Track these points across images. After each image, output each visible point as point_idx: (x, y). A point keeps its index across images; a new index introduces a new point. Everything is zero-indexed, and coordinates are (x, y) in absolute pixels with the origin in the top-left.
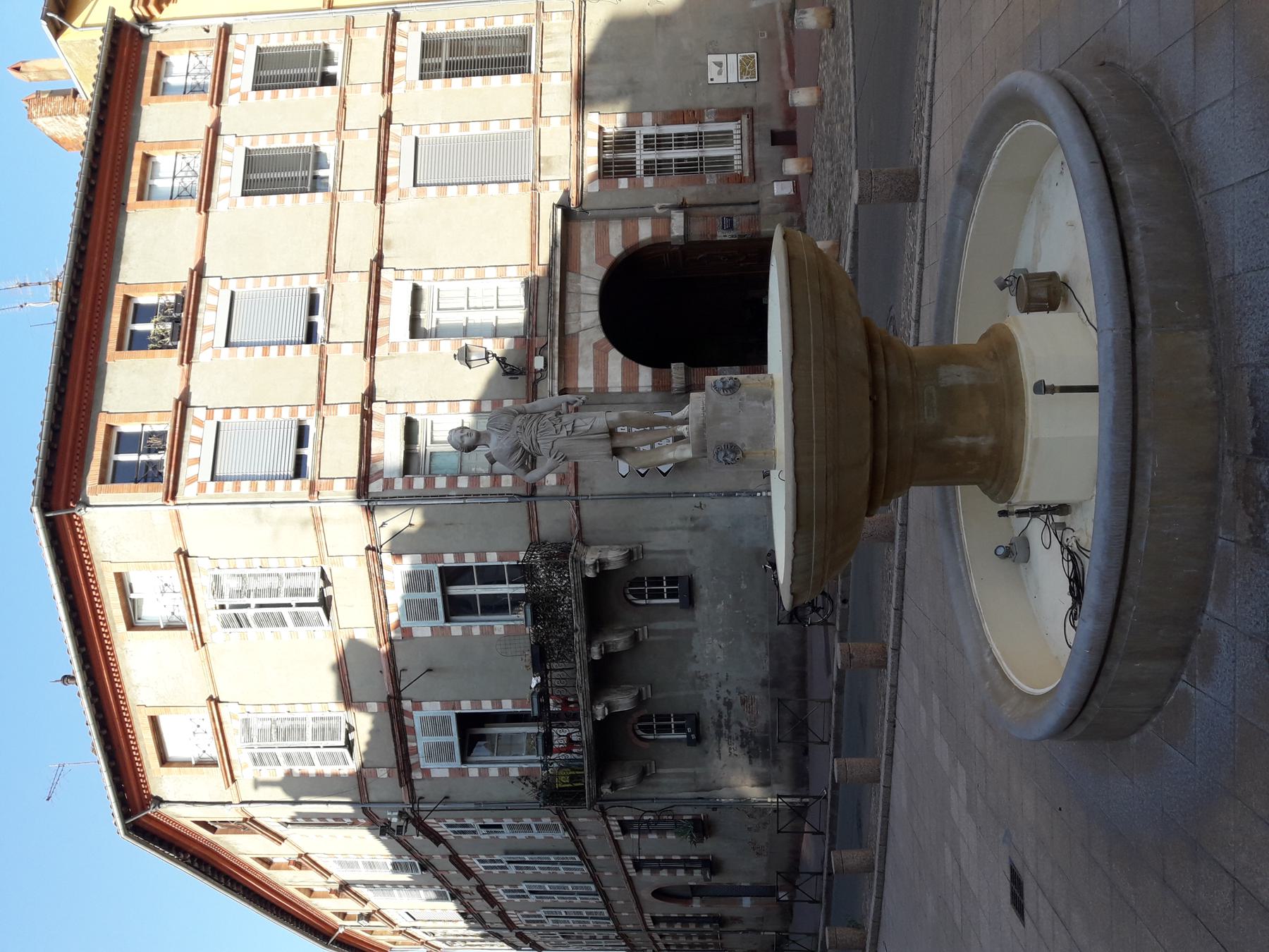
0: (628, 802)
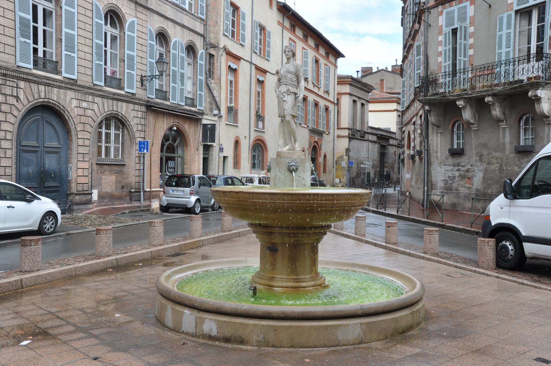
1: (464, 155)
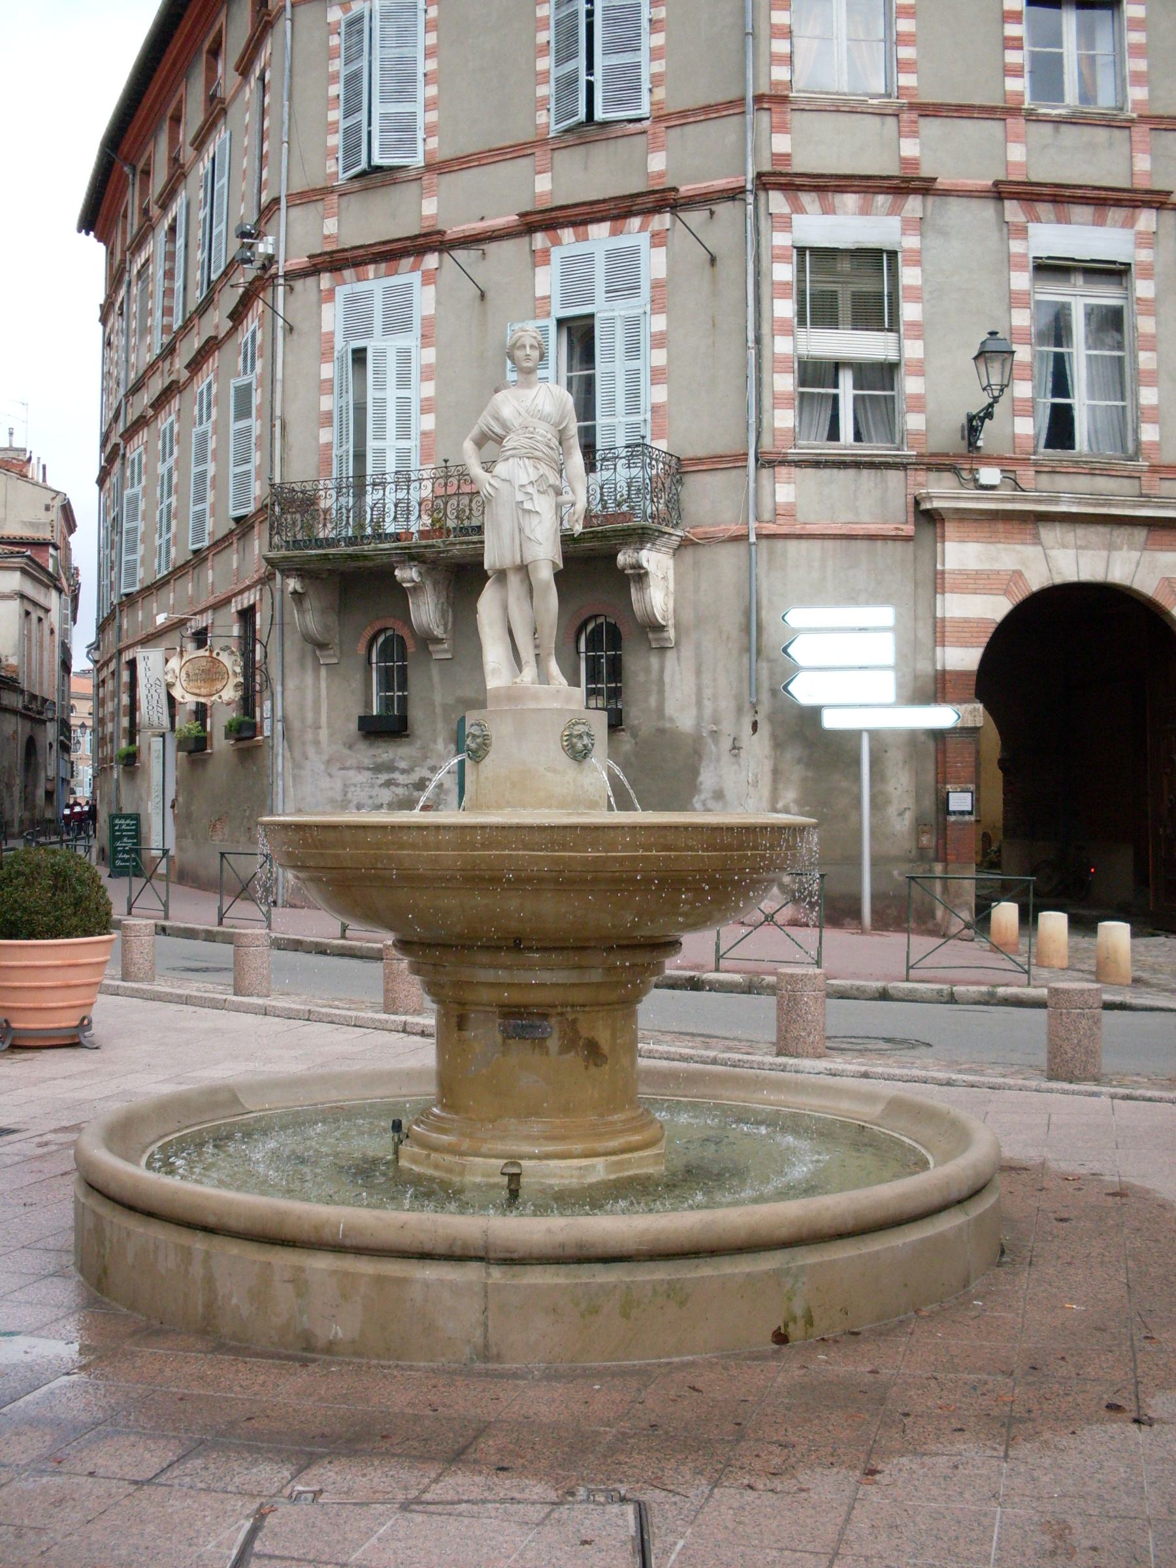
0: (280, 623)
1: (407, 736)
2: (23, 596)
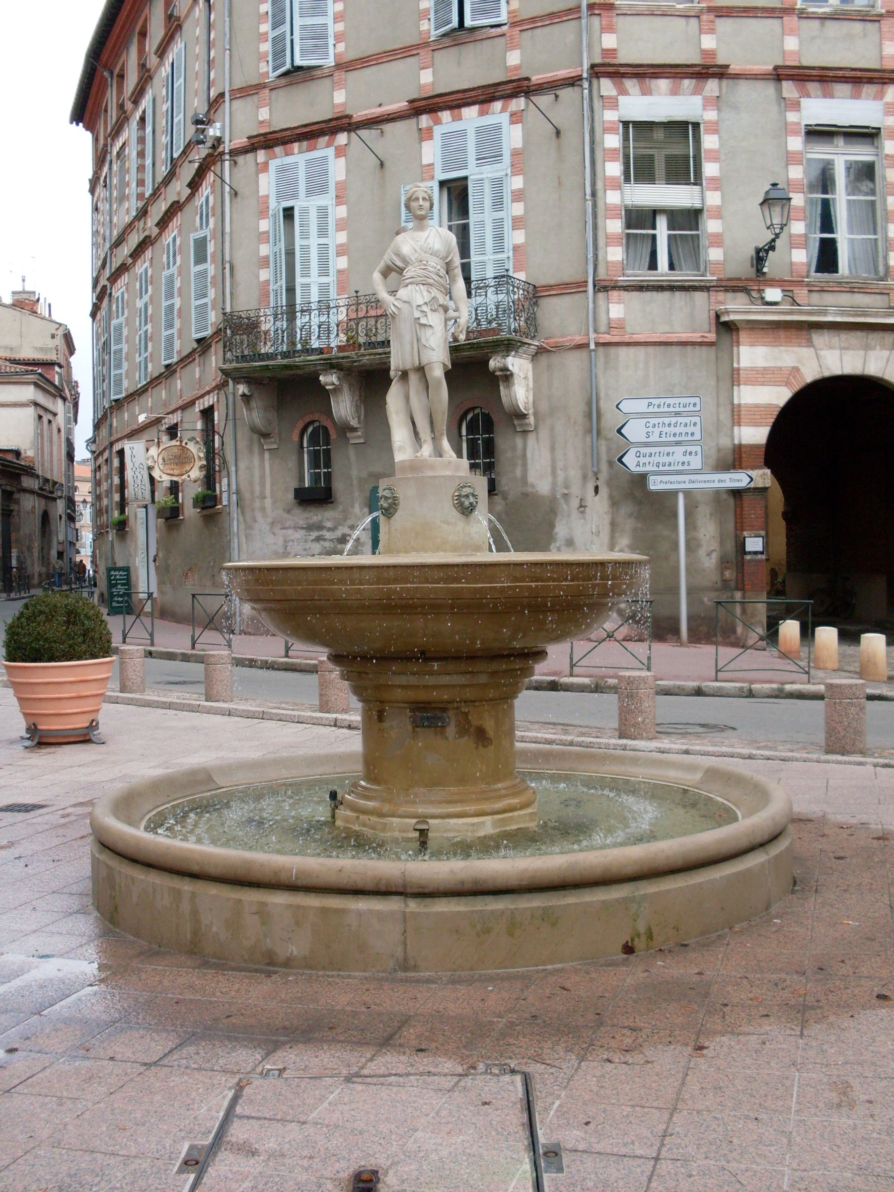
0: (233, 418)
1: (332, 503)
2: (36, 404)
